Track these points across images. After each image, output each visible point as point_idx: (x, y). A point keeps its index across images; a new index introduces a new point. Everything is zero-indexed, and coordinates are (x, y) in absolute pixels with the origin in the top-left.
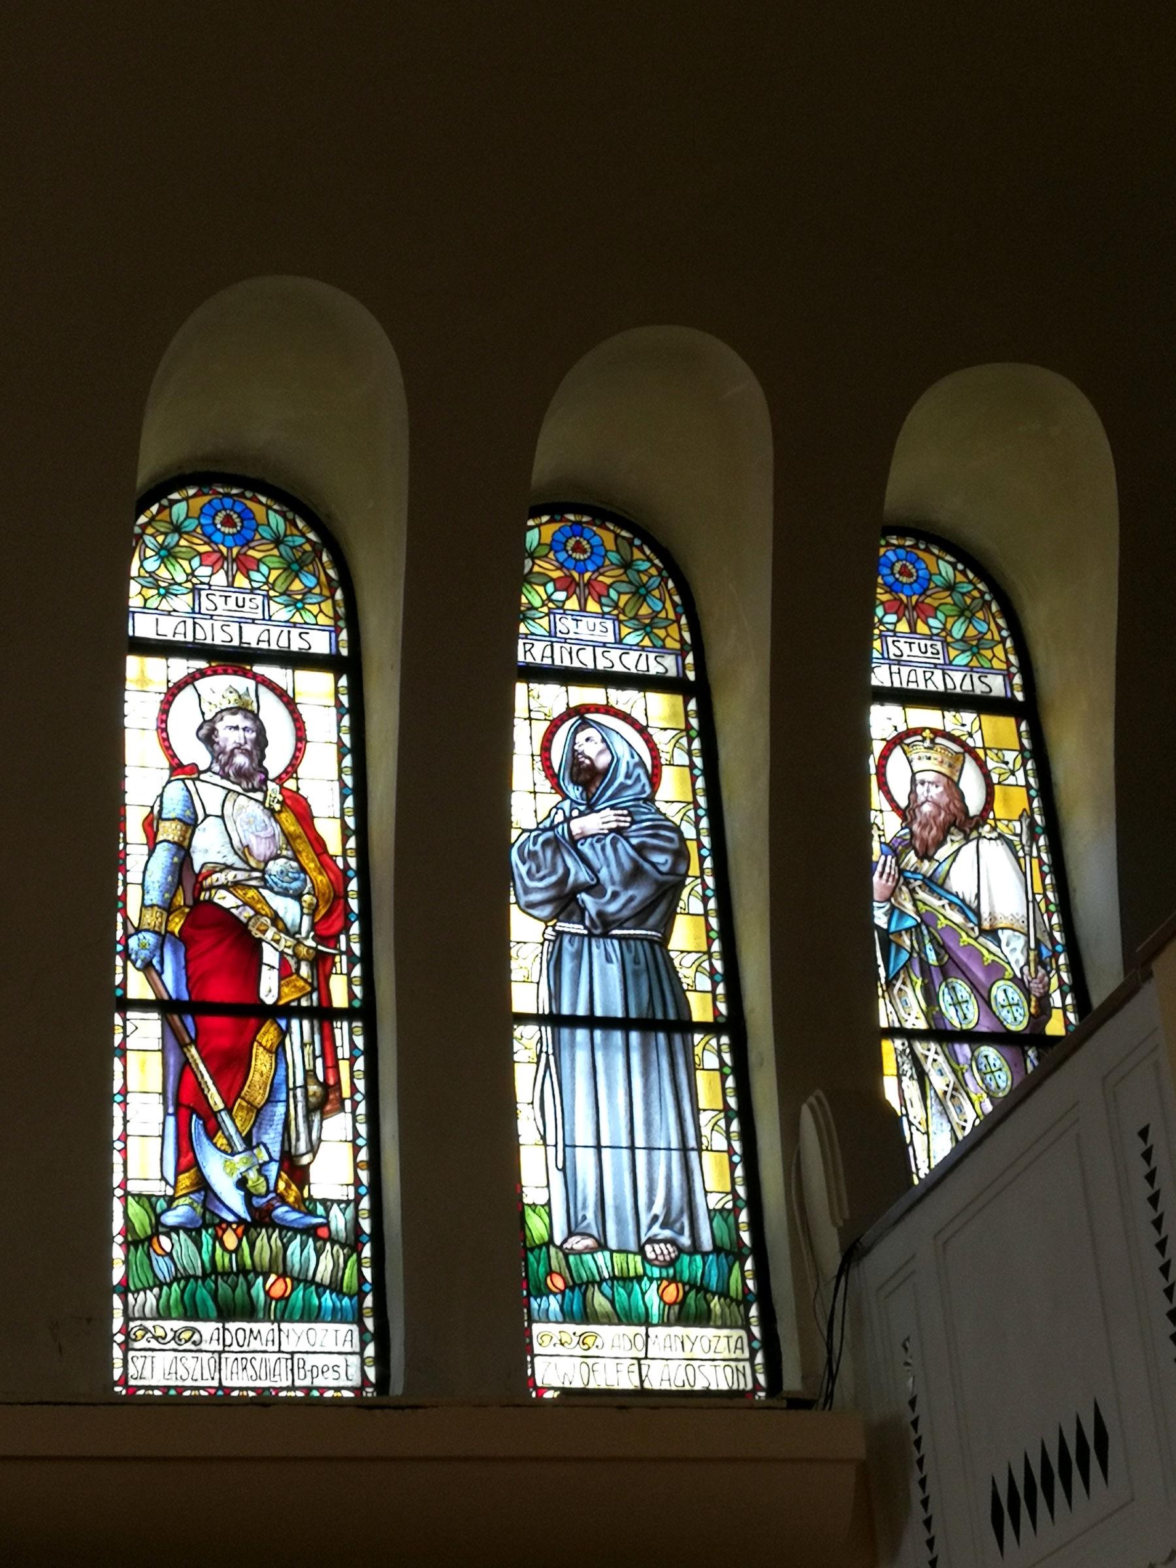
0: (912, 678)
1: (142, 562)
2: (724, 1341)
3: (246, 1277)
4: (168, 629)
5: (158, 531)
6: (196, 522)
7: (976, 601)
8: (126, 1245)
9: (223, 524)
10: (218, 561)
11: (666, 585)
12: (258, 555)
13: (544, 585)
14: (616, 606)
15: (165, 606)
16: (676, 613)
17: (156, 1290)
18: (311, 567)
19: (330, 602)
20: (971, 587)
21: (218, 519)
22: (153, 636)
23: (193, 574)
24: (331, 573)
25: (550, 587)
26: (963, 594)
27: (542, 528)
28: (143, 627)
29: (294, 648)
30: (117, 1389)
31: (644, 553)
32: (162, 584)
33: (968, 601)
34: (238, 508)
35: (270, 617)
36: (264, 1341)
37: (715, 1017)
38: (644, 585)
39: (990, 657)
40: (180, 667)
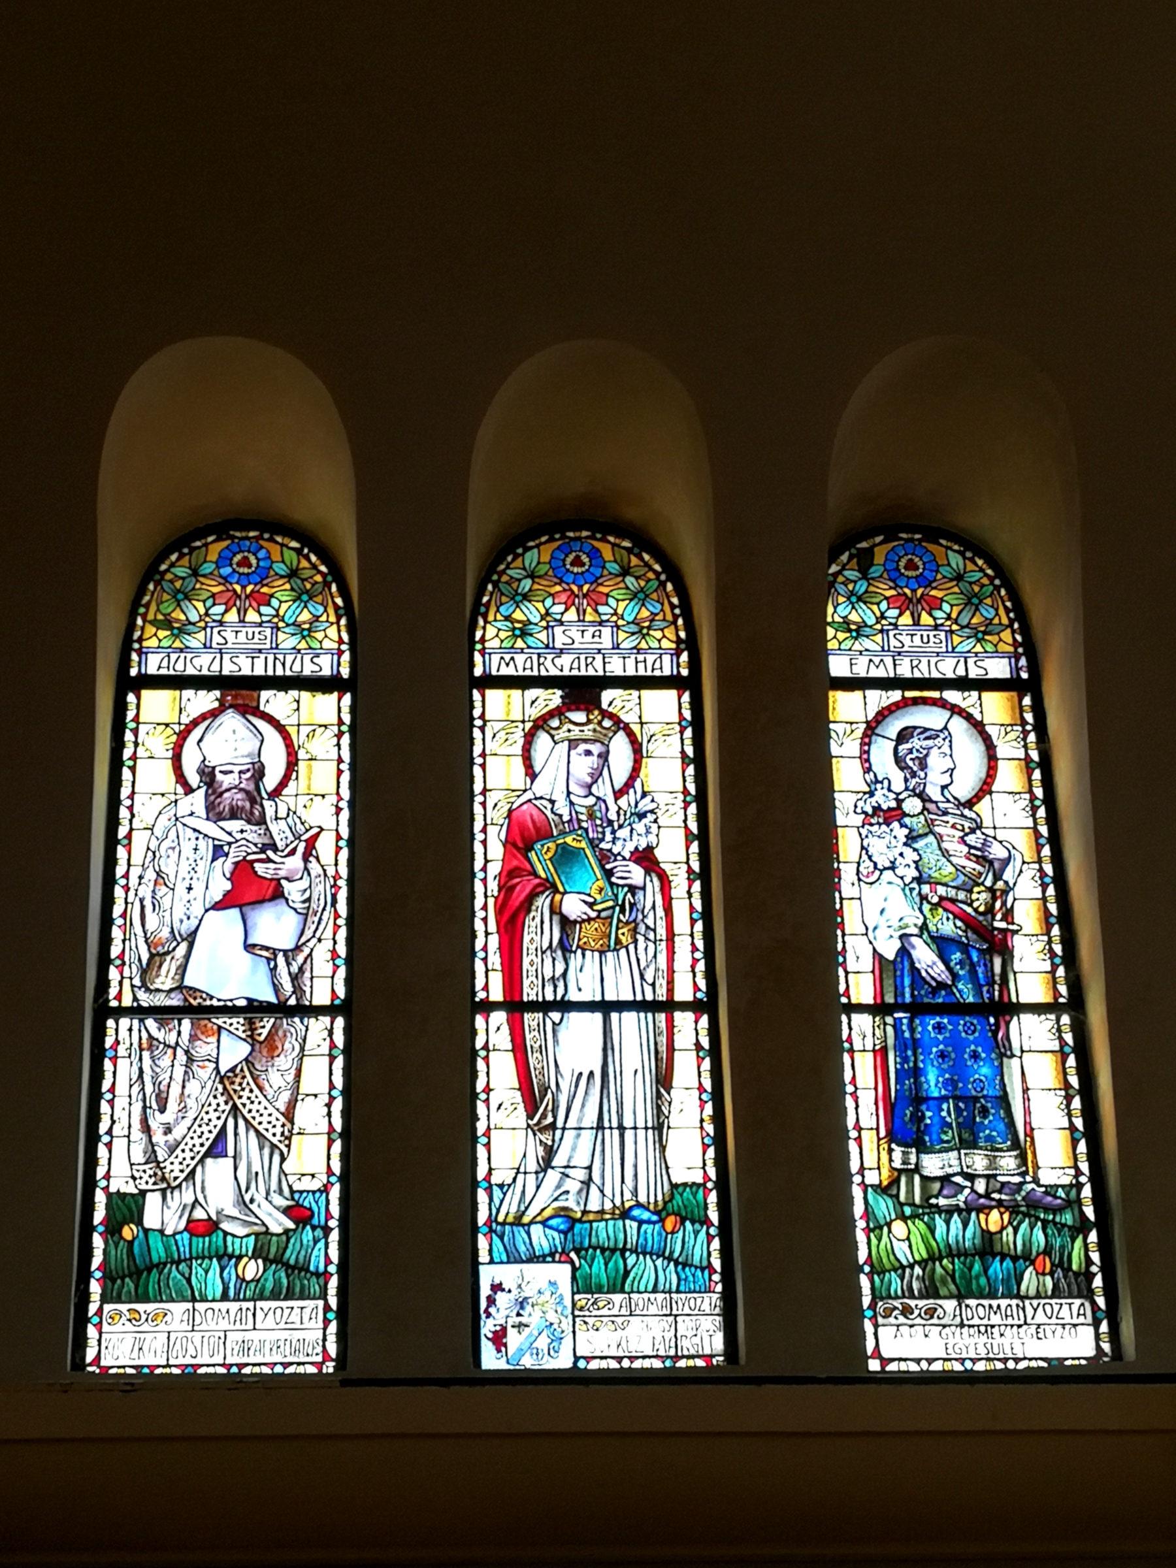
0: (657, 665)
1: (158, 606)
2: (297, 1311)
3: (219, 1261)
4: (520, 666)
5: (512, 578)
6: (882, 569)
7: (650, 584)
8: (868, 1230)
9: (906, 568)
10: (905, 604)
11: (999, 593)
12: (939, 594)
13: (878, 604)
14: (615, 614)
15: (857, 646)
16: (1009, 618)
17: (900, 1271)
18: (320, 597)
19: (1009, 631)
20: (981, 574)
21: (902, 564)
22: (850, 675)
23: (883, 617)
24: (1008, 604)
25: (884, 605)
26: (971, 583)
27: (542, 547)
28: (838, 667)
29: (225, 672)
30: (90, 1369)
31: (976, 564)
32: (853, 627)
33: (976, 589)
34: (587, 549)
35: (954, 648)
36: (232, 1321)
37: (332, 1000)
38: (976, 595)
39: (664, 640)
40: (877, 699)
